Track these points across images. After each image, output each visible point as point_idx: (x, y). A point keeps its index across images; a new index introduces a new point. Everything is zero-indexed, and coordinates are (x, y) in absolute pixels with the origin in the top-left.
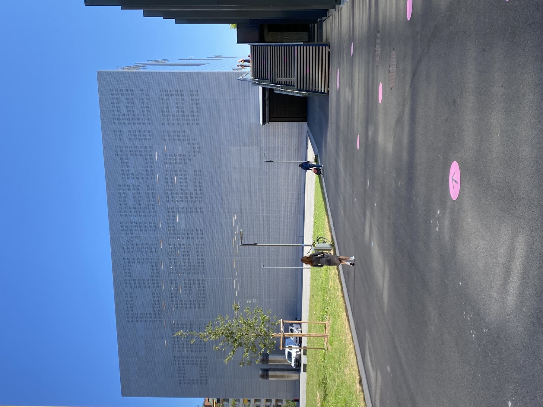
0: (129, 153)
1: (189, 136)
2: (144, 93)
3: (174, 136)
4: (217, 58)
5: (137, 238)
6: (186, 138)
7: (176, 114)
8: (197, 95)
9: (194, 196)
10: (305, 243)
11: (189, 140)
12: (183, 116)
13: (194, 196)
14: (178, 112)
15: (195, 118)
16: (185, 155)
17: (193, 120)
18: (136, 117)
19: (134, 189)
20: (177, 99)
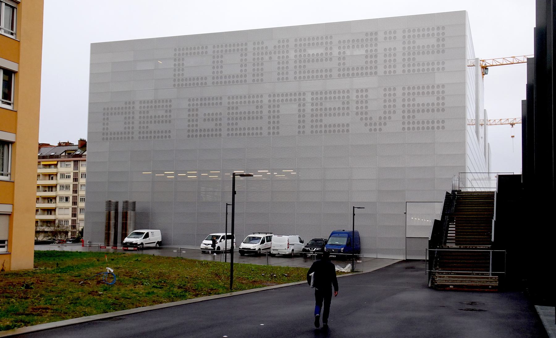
0: (281, 55)
1: (390, 118)
2: (441, 66)
3: (390, 101)
4: (61, 166)
5: (270, 58)
6: (387, 115)
7: (255, 110)
8: (438, 128)
9: (234, 127)
10: (425, 259)
11: (385, 118)
12: (414, 111)
13: (319, 124)
14: (241, 113)
15: (411, 126)
16: (366, 113)
17: (409, 123)
18: (302, 64)
19: (438, 46)
20: (433, 104)
